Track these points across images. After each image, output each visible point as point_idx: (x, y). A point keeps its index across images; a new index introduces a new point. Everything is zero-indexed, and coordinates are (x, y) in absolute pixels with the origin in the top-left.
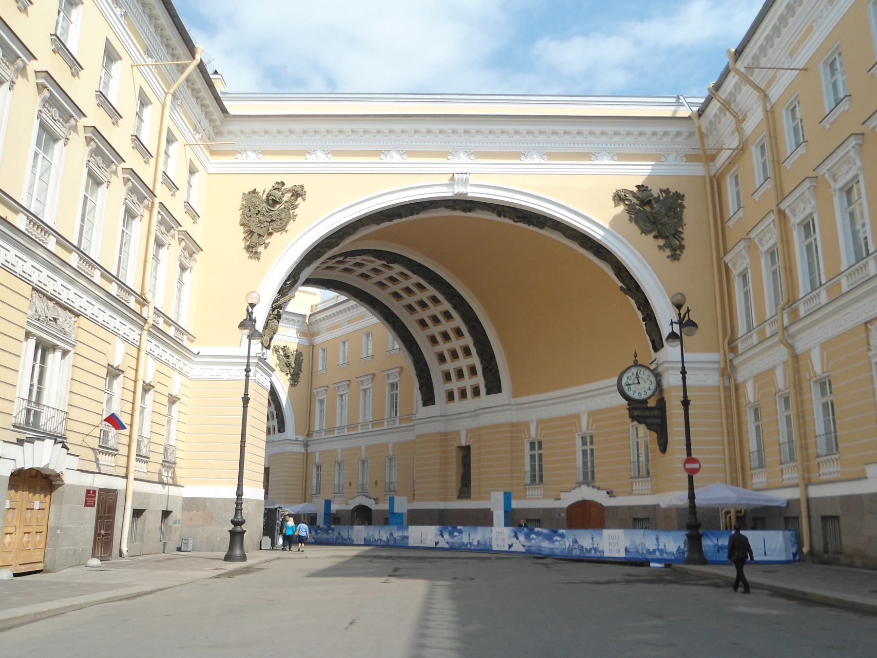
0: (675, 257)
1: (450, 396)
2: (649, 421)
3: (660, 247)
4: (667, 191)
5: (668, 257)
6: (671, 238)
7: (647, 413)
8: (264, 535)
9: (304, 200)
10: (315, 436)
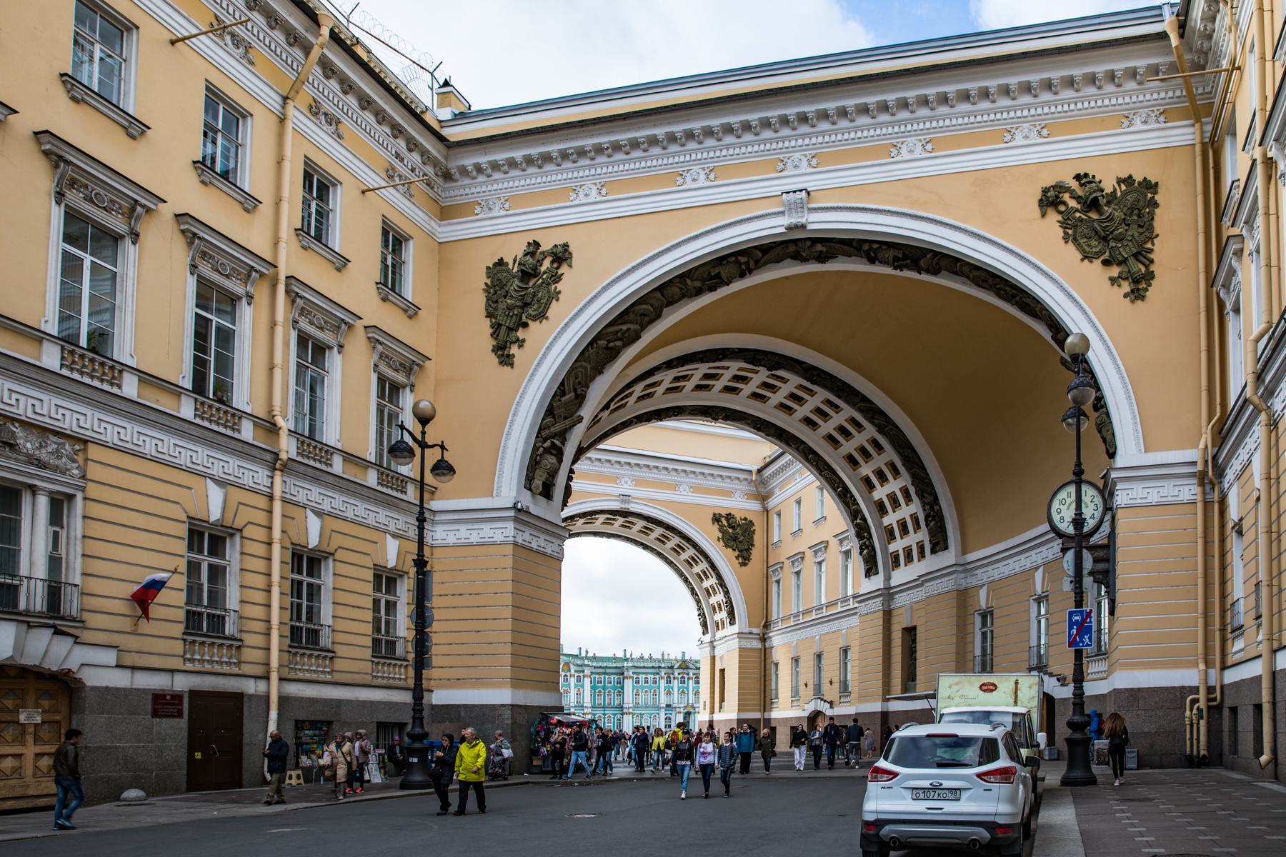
0: (1137, 294)
3: (1113, 280)
4: (1129, 180)
5: (1126, 296)
6: (1132, 261)
8: (118, 799)
9: (570, 266)
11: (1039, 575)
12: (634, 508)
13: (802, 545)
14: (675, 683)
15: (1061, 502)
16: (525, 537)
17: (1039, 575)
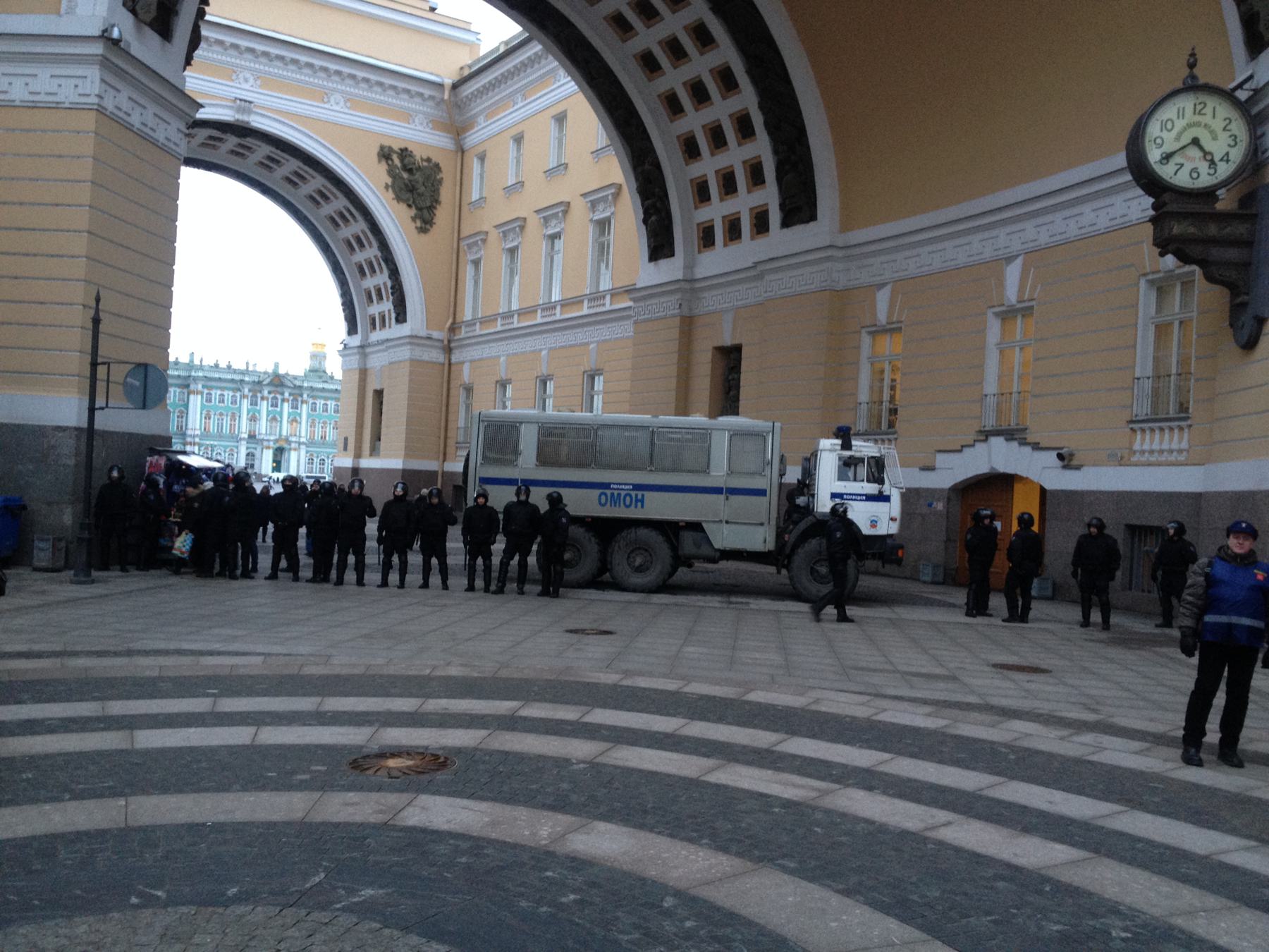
1: (707, 238)
2: (1216, 253)
7: (1212, 230)
10: (463, 333)
11: (1013, 273)
12: (258, 122)
13: (524, 207)
14: (264, 407)
15: (1163, 126)
16: (120, 100)
17: (1013, 273)
